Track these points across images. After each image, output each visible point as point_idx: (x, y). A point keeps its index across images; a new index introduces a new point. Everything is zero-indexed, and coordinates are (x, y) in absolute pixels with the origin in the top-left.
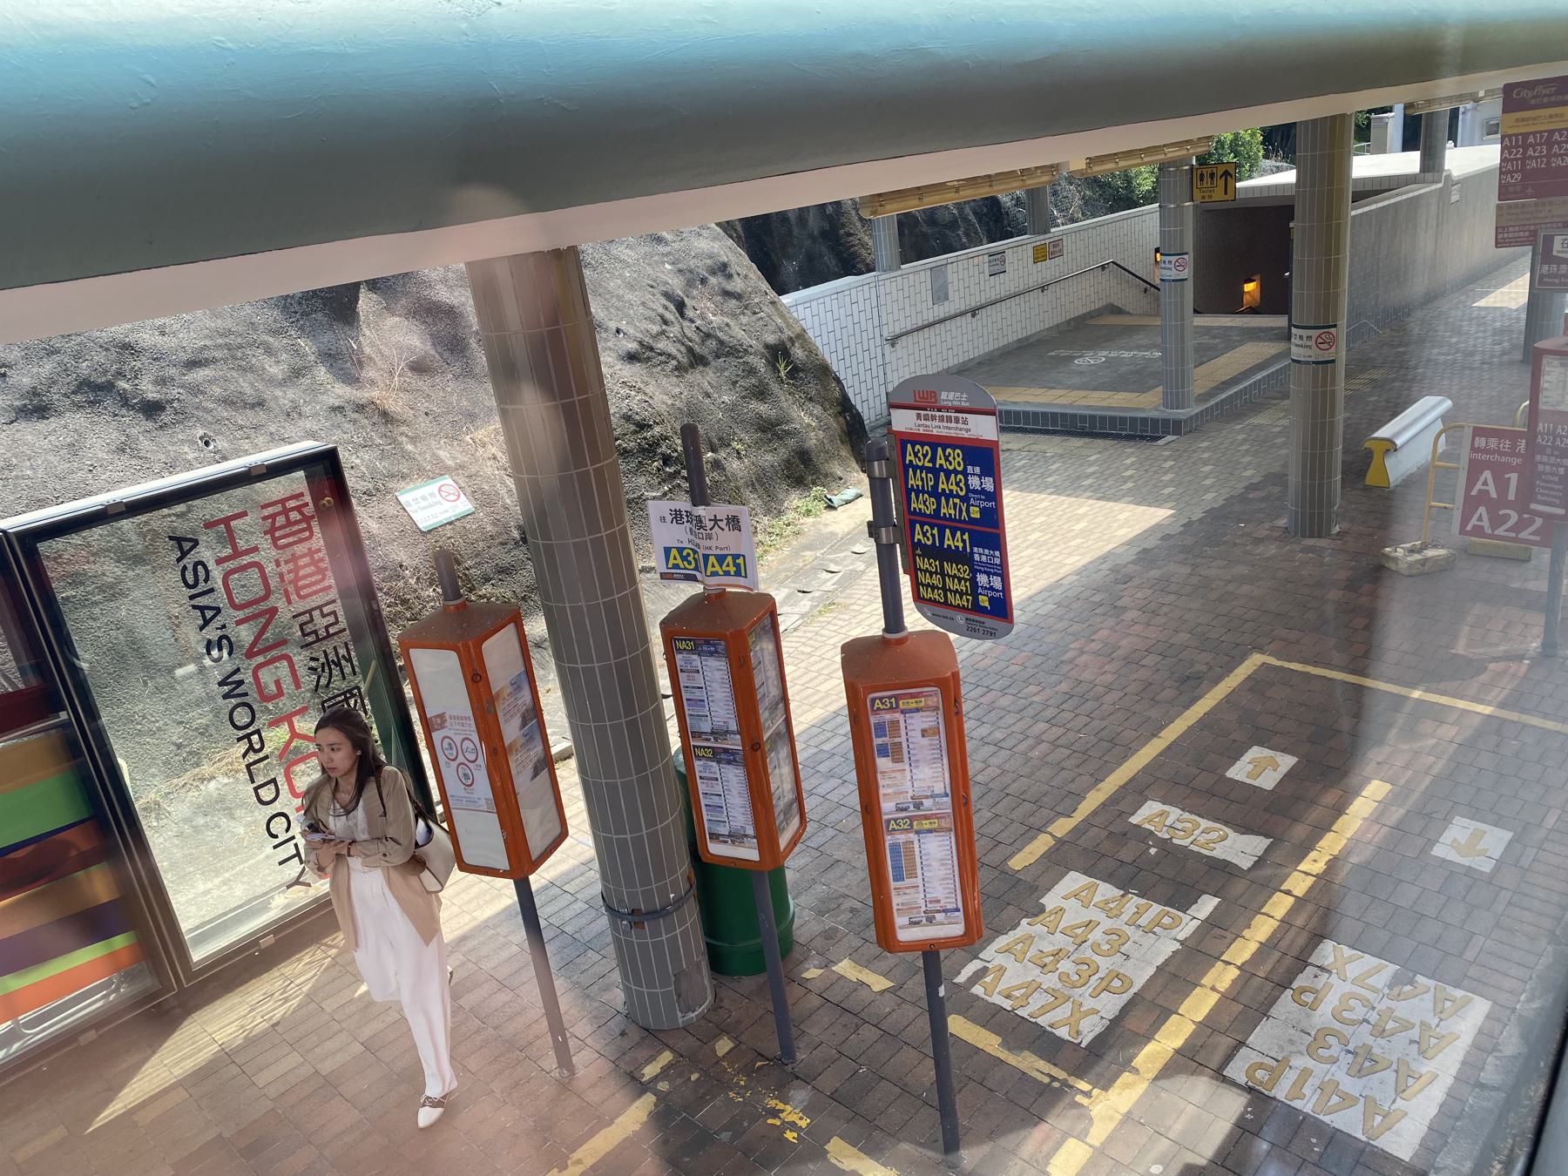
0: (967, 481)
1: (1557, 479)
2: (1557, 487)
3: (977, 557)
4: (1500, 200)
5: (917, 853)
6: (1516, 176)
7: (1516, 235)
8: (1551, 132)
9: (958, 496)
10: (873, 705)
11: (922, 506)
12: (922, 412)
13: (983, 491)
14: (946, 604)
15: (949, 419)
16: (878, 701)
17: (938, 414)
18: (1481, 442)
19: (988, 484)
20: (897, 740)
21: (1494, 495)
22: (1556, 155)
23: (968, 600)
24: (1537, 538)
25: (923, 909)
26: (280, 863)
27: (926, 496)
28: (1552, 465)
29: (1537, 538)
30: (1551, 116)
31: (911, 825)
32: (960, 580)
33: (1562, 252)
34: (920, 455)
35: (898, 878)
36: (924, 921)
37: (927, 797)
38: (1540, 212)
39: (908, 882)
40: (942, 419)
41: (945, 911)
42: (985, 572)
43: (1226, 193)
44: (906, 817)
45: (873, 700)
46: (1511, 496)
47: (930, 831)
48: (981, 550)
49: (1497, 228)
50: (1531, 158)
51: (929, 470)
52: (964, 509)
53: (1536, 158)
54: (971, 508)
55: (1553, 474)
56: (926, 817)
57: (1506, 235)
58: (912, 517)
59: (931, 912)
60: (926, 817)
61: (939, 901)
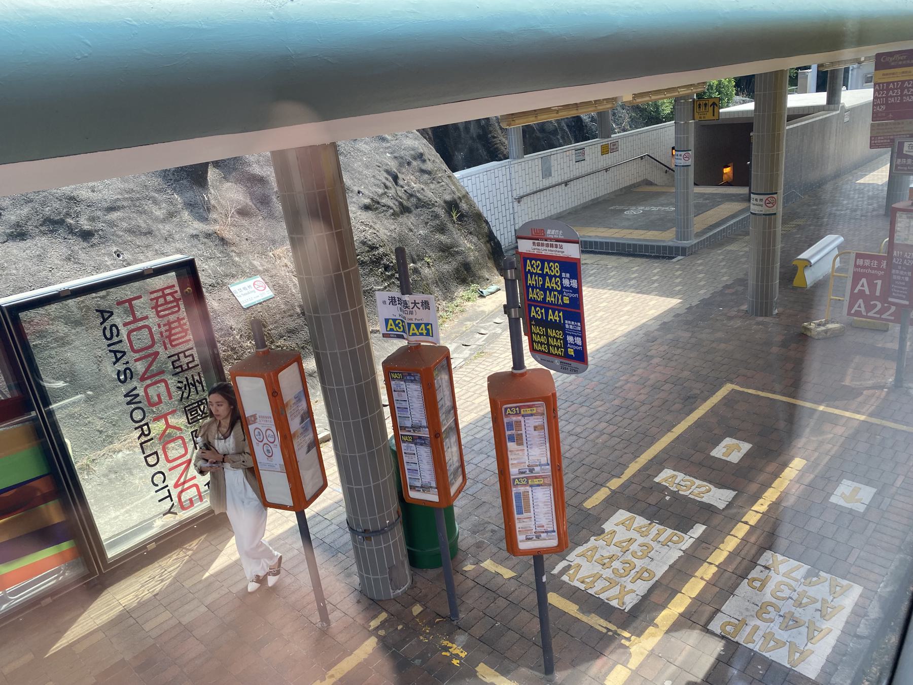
0: (562, 281)
1: (904, 284)
2: (904, 288)
3: (567, 326)
5: (531, 498)
6: (882, 107)
7: (882, 141)
8: (903, 82)
9: (556, 290)
10: (506, 412)
11: (535, 296)
12: (536, 241)
13: (571, 288)
14: (549, 353)
15: (552, 246)
16: (509, 409)
17: (545, 242)
19: (574, 284)
20: (519, 432)
21: (867, 292)
24: (893, 318)
25: (534, 530)
26: (160, 501)
27: (538, 290)
28: (902, 276)
29: (893, 318)
30: (903, 72)
31: (527, 482)
32: (557, 339)
33: (909, 152)
34: (534, 266)
35: (520, 513)
36: (534, 538)
39: (525, 515)
41: (547, 532)
42: (572, 335)
43: (714, 115)
44: (525, 477)
45: (506, 409)
46: (878, 294)
47: (538, 485)
48: (569, 322)
49: (871, 137)
50: (891, 97)
51: (539, 275)
52: (560, 298)
54: (564, 298)
55: (902, 281)
56: (536, 477)
57: (876, 142)
60: (536, 477)
61: (543, 526)
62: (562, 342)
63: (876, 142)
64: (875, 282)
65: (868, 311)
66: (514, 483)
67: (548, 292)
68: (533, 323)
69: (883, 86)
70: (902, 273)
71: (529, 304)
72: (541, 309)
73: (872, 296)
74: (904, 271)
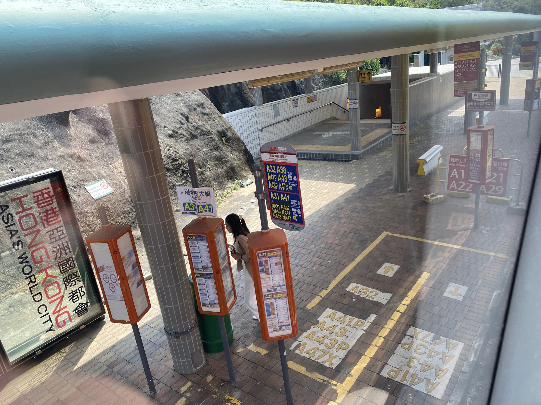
0: (287, 177)
1: (476, 171)
2: (476, 174)
3: (292, 203)
6: (459, 74)
7: (460, 93)
8: (470, 60)
9: (285, 182)
10: (258, 255)
11: (273, 186)
12: (272, 154)
13: (293, 181)
14: (282, 219)
15: (281, 156)
17: (277, 155)
18: (452, 160)
19: (295, 178)
20: (267, 267)
21: (457, 177)
22: (471, 67)
23: (289, 218)
24: (471, 191)
25: (278, 325)
28: (475, 167)
29: (471, 191)
31: (273, 296)
32: (286, 211)
35: (269, 315)
36: (278, 330)
37: (278, 286)
38: (467, 85)
39: (272, 316)
40: (278, 156)
41: (285, 326)
42: (295, 208)
43: (369, 79)
44: (271, 294)
46: (463, 177)
47: (279, 298)
48: (293, 201)
50: (464, 68)
51: (275, 174)
54: (289, 186)
55: (475, 170)
56: (278, 293)
58: (269, 190)
59: (281, 326)
60: (278, 293)
61: (283, 322)
62: (289, 212)
63: (457, 93)
64: (461, 171)
65: (458, 187)
68: (272, 202)
69: (459, 63)
70: (475, 165)
71: (269, 191)
72: (277, 194)
74: (476, 164)
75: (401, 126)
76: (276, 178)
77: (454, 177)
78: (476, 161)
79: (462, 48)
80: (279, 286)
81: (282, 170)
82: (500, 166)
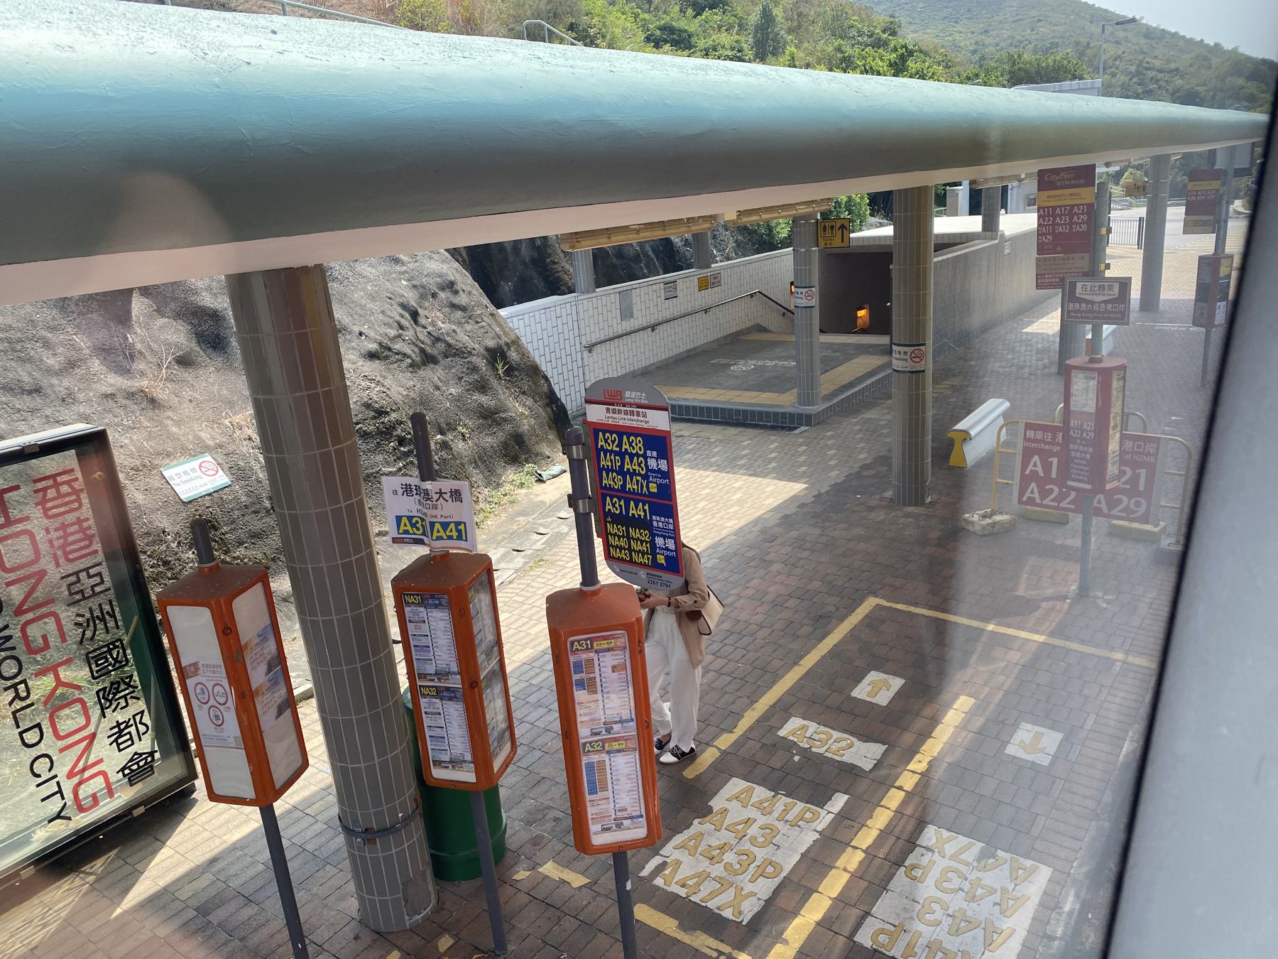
0: (646, 462)
3: (655, 524)
4: (1038, 254)
7: (1050, 280)
8: (1072, 207)
9: (639, 474)
11: (611, 482)
12: (611, 407)
14: (631, 562)
15: (632, 413)
16: (576, 643)
17: (623, 408)
18: (1031, 434)
19: (663, 465)
20: (592, 675)
21: (1041, 474)
23: (648, 558)
24: (1073, 507)
25: (613, 817)
26: (43, 800)
27: (614, 474)
30: (1071, 195)
31: (603, 747)
32: (642, 542)
39: (600, 795)
40: (626, 413)
41: (631, 818)
42: (662, 536)
43: (842, 241)
46: (1054, 475)
47: (619, 751)
49: (1037, 275)
51: (616, 453)
52: (645, 485)
53: (1062, 224)
55: (1082, 459)
56: (615, 740)
60: (615, 740)
61: (626, 810)
66: (584, 749)
67: (628, 476)
68: (609, 519)
69: (1049, 211)
73: (1048, 479)
75: (913, 352)
76: (618, 464)
77: (1034, 473)
78: (1084, 439)
79: (1054, 177)
80: (620, 722)
81: (634, 444)
82: (1137, 453)
